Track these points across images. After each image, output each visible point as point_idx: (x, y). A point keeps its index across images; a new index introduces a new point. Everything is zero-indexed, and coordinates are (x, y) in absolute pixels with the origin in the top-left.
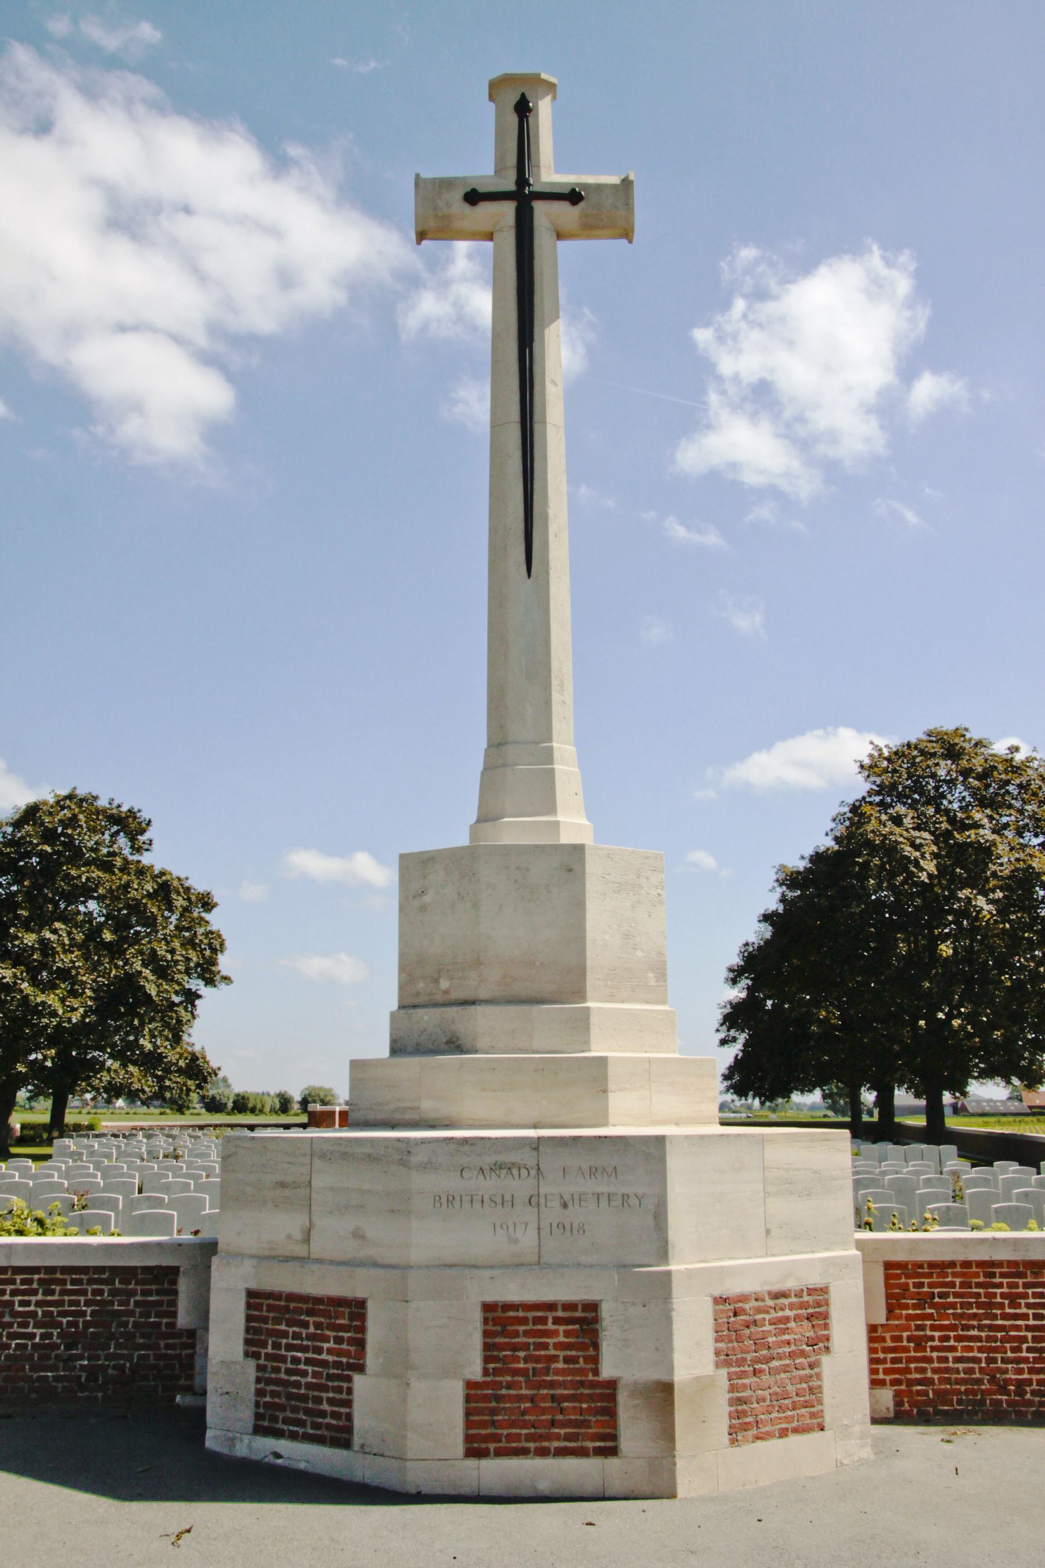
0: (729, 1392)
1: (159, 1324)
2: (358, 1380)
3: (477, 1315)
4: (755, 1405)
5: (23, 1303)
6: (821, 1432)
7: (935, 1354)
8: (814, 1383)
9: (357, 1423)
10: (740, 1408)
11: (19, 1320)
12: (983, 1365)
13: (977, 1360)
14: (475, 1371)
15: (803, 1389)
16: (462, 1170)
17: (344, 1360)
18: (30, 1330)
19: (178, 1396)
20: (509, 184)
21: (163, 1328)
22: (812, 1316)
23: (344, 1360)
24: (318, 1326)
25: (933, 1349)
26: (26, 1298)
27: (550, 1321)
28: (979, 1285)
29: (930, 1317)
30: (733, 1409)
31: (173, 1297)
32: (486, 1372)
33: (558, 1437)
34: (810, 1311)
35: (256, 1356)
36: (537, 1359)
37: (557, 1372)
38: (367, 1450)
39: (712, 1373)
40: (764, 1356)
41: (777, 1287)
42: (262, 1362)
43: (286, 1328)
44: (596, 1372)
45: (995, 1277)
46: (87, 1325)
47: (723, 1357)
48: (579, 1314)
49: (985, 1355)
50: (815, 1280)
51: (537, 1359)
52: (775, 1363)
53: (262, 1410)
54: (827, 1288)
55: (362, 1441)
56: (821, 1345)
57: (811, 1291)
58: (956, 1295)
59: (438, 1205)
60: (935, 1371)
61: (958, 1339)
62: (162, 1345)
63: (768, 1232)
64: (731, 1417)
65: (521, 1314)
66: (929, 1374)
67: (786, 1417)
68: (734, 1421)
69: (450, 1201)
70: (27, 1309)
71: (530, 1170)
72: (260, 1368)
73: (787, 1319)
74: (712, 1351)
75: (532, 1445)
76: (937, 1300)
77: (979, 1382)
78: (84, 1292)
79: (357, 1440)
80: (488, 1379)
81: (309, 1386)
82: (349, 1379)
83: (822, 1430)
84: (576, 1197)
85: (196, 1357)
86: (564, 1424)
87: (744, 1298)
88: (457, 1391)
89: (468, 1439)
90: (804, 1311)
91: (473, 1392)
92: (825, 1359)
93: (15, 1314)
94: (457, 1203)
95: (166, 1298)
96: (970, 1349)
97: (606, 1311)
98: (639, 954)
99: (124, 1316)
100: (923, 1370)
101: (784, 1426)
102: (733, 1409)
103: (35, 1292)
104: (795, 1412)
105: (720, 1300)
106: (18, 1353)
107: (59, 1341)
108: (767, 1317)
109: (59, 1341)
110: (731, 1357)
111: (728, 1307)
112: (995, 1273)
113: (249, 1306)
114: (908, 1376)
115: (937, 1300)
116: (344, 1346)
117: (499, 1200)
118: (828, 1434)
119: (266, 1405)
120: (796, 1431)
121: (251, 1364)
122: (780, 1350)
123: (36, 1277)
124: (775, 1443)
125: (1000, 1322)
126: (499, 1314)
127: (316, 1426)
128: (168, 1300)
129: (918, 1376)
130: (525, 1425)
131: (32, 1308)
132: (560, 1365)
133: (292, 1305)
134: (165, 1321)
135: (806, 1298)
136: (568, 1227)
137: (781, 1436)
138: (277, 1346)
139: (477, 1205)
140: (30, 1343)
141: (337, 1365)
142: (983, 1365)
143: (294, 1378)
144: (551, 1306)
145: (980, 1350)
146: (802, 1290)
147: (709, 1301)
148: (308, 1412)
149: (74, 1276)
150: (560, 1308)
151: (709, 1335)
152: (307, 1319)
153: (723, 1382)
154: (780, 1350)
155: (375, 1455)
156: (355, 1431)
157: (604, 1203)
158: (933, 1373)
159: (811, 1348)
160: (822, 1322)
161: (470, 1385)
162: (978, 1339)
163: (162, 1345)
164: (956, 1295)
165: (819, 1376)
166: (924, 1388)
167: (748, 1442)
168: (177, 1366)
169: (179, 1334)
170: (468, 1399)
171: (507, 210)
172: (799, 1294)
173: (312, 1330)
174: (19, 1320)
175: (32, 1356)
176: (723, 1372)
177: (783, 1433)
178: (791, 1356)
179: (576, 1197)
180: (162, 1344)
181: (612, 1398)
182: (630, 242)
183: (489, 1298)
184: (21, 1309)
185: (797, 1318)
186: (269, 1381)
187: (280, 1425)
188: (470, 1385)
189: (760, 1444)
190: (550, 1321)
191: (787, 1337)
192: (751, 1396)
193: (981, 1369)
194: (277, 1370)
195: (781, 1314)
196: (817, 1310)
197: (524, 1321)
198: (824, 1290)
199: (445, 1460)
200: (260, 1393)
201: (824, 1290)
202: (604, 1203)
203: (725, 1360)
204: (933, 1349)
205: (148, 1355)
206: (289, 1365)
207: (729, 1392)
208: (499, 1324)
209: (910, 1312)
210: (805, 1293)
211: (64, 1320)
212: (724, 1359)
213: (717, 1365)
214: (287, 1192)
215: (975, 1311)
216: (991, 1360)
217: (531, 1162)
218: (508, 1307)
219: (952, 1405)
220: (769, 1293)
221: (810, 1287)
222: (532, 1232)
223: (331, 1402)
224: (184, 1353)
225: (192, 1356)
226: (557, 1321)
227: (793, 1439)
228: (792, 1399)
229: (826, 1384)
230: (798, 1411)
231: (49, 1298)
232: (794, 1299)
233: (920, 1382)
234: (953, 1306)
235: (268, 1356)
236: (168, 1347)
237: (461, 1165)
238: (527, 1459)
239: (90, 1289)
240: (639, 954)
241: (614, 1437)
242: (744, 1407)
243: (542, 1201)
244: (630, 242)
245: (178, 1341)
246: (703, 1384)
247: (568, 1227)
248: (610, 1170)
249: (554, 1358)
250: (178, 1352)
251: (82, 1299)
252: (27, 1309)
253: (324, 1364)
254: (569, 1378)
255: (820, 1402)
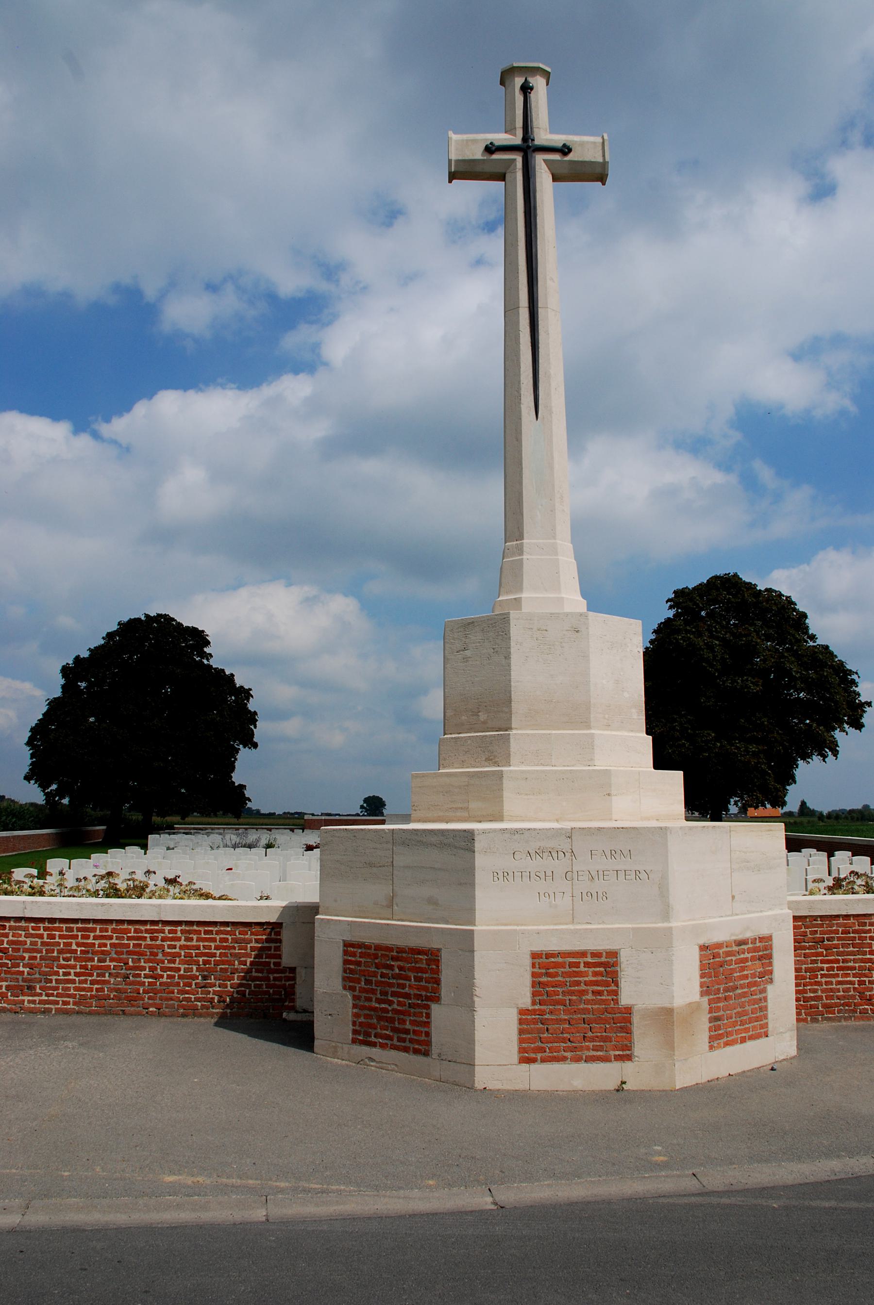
0: (709, 1013)
1: (269, 963)
2: (434, 1007)
3: (528, 961)
4: (726, 1021)
5: (169, 947)
6: (767, 1038)
7: (823, 980)
8: (763, 1004)
9: (434, 1039)
10: (716, 1023)
11: (169, 958)
12: (856, 986)
13: (853, 983)
14: (526, 1001)
15: (756, 1008)
16: (514, 854)
17: (424, 993)
18: (176, 965)
19: (284, 1013)
20: (516, 139)
21: (272, 966)
22: (762, 957)
23: (424, 993)
24: (401, 968)
25: (823, 976)
26: (173, 943)
27: (582, 965)
28: (854, 932)
29: (821, 954)
30: (712, 1024)
31: (278, 944)
32: (534, 1003)
33: (588, 1049)
34: (761, 953)
35: (353, 989)
36: (572, 993)
37: (587, 1002)
38: (443, 1057)
39: (698, 1000)
40: (731, 986)
41: (740, 937)
42: (356, 993)
43: (376, 970)
44: (616, 1002)
45: (866, 926)
46: (217, 963)
47: (705, 989)
48: (603, 959)
49: (858, 979)
50: (764, 932)
51: (572, 993)
52: (739, 991)
53: (357, 1028)
54: (771, 936)
55: (438, 1051)
56: (767, 977)
57: (761, 939)
58: (839, 939)
59: (496, 879)
60: (823, 991)
61: (839, 969)
62: (272, 978)
63: (733, 897)
64: (710, 1030)
65: (560, 960)
66: (819, 993)
67: (745, 1029)
68: (712, 1033)
69: (506, 874)
70: (174, 951)
71: (566, 853)
72: (355, 998)
73: (746, 960)
74: (698, 984)
75: (568, 1054)
76: (826, 942)
77: (853, 997)
78: (214, 940)
79: (435, 1050)
80: (537, 1007)
81: (395, 1011)
82: (428, 1007)
83: (767, 1036)
84: (601, 873)
85: (296, 986)
86: (592, 1039)
87: (719, 945)
88: (513, 1016)
89: (521, 1050)
90: (757, 954)
91: (524, 1017)
92: (769, 987)
93: (165, 954)
94: (510, 878)
95: (273, 945)
96: (847, 975)
97: (623, 957)
98: (626, 695)
99: (243, 957)
100: (815, 991)
101: (743, 1035)
102: (712, 1024)
103: (179, 939)
104: (750, 1025)
105: (703, 948)
106: (169, 980)
107: (198, 974)
108: (734, 958)
109: (198, 974)
110: (710, 988)
111: (709, 952)
112: (866, 923)
113: (345, 953)
114: (805, 995)
115: (826, 942)
116: (423, 983)
117: (542, 875)
118: (770, 1038)
119: (361, 1024)
120: (751, 1038)
121: (349, 995)
122: (742, 982)
123: (179, 928)
124: (738, 1047)
125: (868, 956)
126: (544, 960)
127: (400, 1040)
128: (275, 946)
129: (812, 995)
130: (564, 1040)
131: (177, 950)
132: (590, 997)
133: (380, 953)
134: (272, 961)
135: (758, 944)
136: (595, 895)
137: (741, 1042)
138: (368, 982)
139: (526, 879)
140: (177, 975)
141: (418, 996)
142: (856, 986)
143: (383, 1006)
144: (583, 954)
145: (854, 976)
146: (756, 939)
147: (697, 949)
148: (394, 1030)
149: (206, 928)
150: (589, 955)
151: (696, 973)
152: (392, 963)
153: (706, 1006)
154: (742, 982)
155: (449, 1061)
156: (433, 1044)
157: (621, 875)
158: (822, 993)
159: (760, 979)
160: (768, 961)
161: (522, 1012)
162: (854, 968)
163: (272, 978)
164: (839, 939)
165: (765, 999)
166: (816, 1003)
167: (721, 1047)
168: (283, 993)
169: (283, 971)
170: (521, 1022)
171: (519, 159)
172: (754, 941)
173: (397, 971)
174: (169, 958)
175: (178, 984)
176: (706, 999)
177: (743, 1040)
178: (749, 985)
179: (601, 873)
180: (271, 977)
181: (629, 1021)
182: (604, 184)
183: (537, 948)
184: (169, 950)
185: (753, 959)
186: (363, 1008)
187: (373, 1039)
188: (522, 1012)
189: (729, 1049)
190: (582, 965)
191: (745, 973)
192: (723, 1015)
193: (854, 989)
194: (369, 999)
195: (742, 956)
196: (765, 953)
197: (562, 965)
198: (769, 938)
199: (504, 1065)
200: (356, 1015)
201: (769, 938)
202: (621, 875)
203: (707, 990)
204: (823, 976)
205: (262, 985)
206: (379, 996)
207: (709, 1013)
208: (543, 968)
209: (807, 951)
210: (757, 941)
211: (201, 959)
212: (706, 990)
213: (702, 994)
214: (375, 870)
215: (852, 949)
216: (861, 983)
217: (566, 847)
218: (549, 955)
219: (835, 1014)
220: (735, 941)
221: (760, 936)
222: (568, 898)
223: (413, 1023)
224: (287, 983)
225: (293, 986)
226: (587, 965)
227: (750, 1044)
228: (748, 1016)
229: (770, 1004)
230: (752, 1024)
231: (189, 943)
232: (750, 946)
233: (812, 999)
234: (837, 946)
235: (362, 990)
236: (275, 979)
237: (513, 849)
238: (565, 1064)
239: (218, 938)
240: (626, 695)
241: (629, 1048)
242: (719, 1023)
243: (575, 877)
244: (604, 184)
245: (283, 975)
246: (693, 1008)
247: (595, 895)
248: (626, 852)
249: (583, 993)
250: (283, 982)
251: (213, 944)
252: (174, 951)
253: (407, 996)
254: (597, 1006)
255: (766, 1017)
